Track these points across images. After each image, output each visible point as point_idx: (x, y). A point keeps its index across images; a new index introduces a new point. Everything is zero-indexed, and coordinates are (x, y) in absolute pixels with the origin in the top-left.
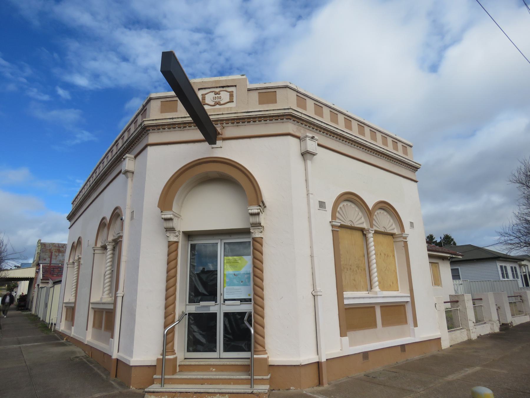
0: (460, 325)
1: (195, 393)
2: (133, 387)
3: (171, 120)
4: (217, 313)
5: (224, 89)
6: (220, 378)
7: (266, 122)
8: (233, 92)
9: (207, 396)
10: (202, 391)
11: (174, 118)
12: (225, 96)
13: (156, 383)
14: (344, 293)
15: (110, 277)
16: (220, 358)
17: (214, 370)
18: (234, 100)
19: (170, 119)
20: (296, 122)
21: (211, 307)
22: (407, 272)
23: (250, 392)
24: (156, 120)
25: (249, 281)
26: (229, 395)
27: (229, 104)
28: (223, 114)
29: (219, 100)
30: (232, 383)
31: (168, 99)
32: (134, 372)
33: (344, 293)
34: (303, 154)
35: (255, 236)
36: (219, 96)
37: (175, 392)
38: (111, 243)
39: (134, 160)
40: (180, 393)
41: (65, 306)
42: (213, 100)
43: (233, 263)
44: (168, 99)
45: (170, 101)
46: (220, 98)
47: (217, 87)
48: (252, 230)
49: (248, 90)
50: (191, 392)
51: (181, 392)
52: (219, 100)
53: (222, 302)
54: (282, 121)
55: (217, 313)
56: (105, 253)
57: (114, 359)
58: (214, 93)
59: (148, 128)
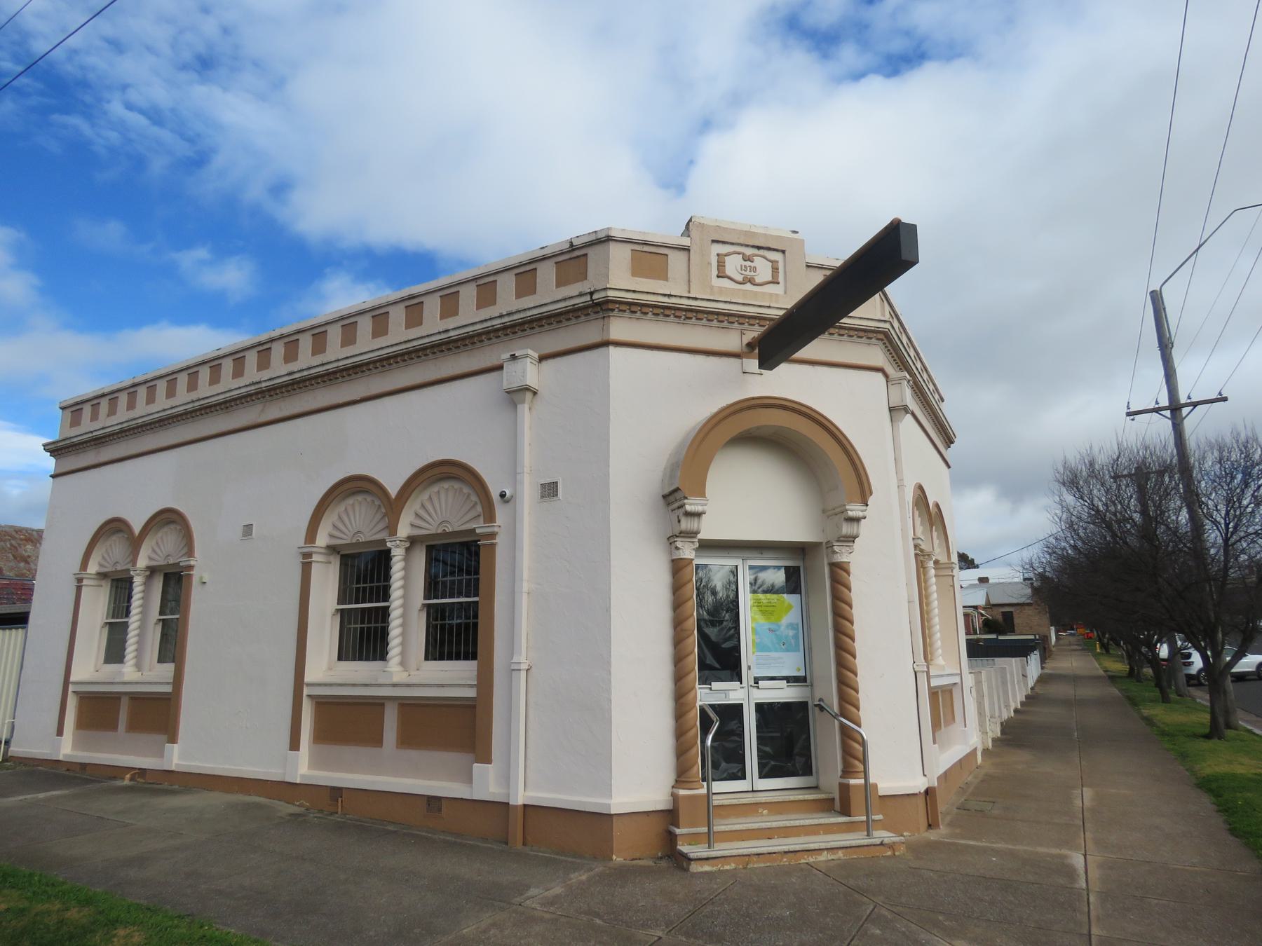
1: (786, 852)
2: (617, 857)
3: (666, 300)
4: (742, 704)
5: (761, 252)
6: (802, 824)
7: (841, 338)
8: (777, 262)
9: (806, 857)
10: (798, 848)
11: (672, 296)
12: (763, 270)
13: (681, 843)
16: (753, 791)
17: (765, 812)
18: (781, 279)
19: (665, 295)
20: (845, 337)
22: (73, 603)
23: (878, 843)
24: (634, 291)
25: (797, 645)
26: (844, 850)
28: (769, 307)
29: (752, 273)
30: (822, 832)
31: (646, 248)
32: (617, 825)
34: (891, 410)
35: (842, 560)
37: (749, 855)
38: (403, 543)
39: (537, 364)
40: (757, 856)
41: (74, 692)
42: (740, 272)
43: (767, 606)
44: (646, 248)
45: (650, 253)
46: (754, 269)
47: (747, 246)
48: (838, 547)
49: (806, 266)
50: (779, 853)
51: (758, 854)
52: (752, 273)
54: (868, 341)
55: (742, 704)
56: (333, 563)
57: (520, 805)
58: (741, 255)
59: (611, 306)
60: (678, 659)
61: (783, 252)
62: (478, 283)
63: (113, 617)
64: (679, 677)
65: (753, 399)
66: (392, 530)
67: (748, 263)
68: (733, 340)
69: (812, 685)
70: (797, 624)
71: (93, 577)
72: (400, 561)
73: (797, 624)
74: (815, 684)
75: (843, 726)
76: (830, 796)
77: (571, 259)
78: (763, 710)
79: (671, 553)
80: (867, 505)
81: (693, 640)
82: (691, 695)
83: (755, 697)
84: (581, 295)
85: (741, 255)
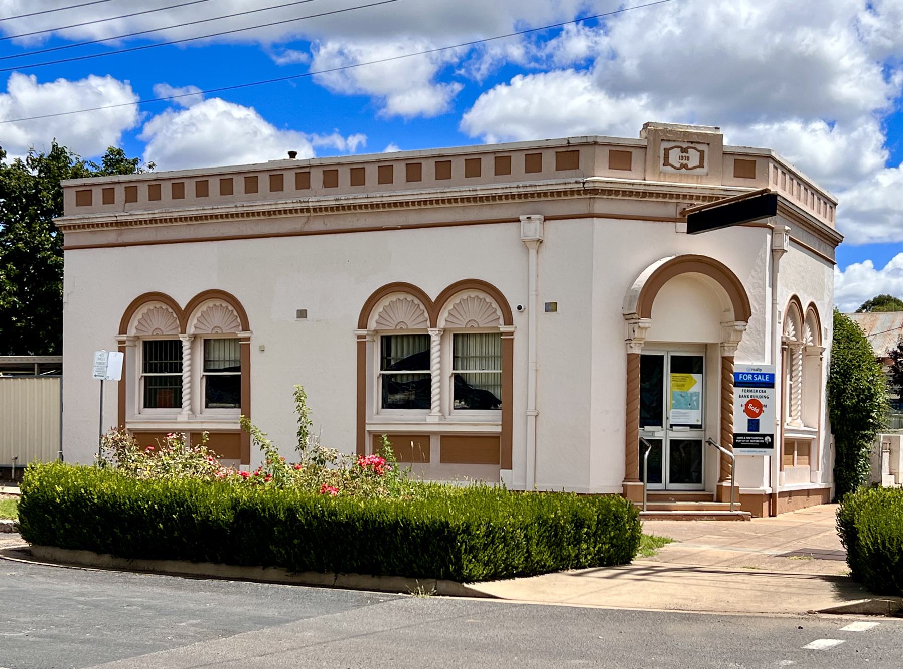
0: (195, 622)
5: (693, 145)
14: (500, 427)
15: (190, 393)
21: (658, 433)
27: (698, 169)
29: (686, 162)
33: (501, 431)
36: (687, 155)
53: (668, 427)
58: (680, 149)
60: (629, 412)
61: (708, 144)
62: (496, 156)
63: (146, 372)
64: (628, 423)
65: (682, 256)
66: (434, 325)
67: (684, 155)
68: (671, 210)
69: (705, 430)
70: (699, 393)
71: (132, 339)
72: (437, 345)
73: (699, 393)
74: (707, 430)
75: (722, 453)
76: (712, 493)
77: (567, 151)
78: (674, 444)
79: (626, 349)
80: (747, 322)
81: (638, 402)
82: (635, 433)
83: (670, 436)
84: (577, 182)
85: (680, 149)
